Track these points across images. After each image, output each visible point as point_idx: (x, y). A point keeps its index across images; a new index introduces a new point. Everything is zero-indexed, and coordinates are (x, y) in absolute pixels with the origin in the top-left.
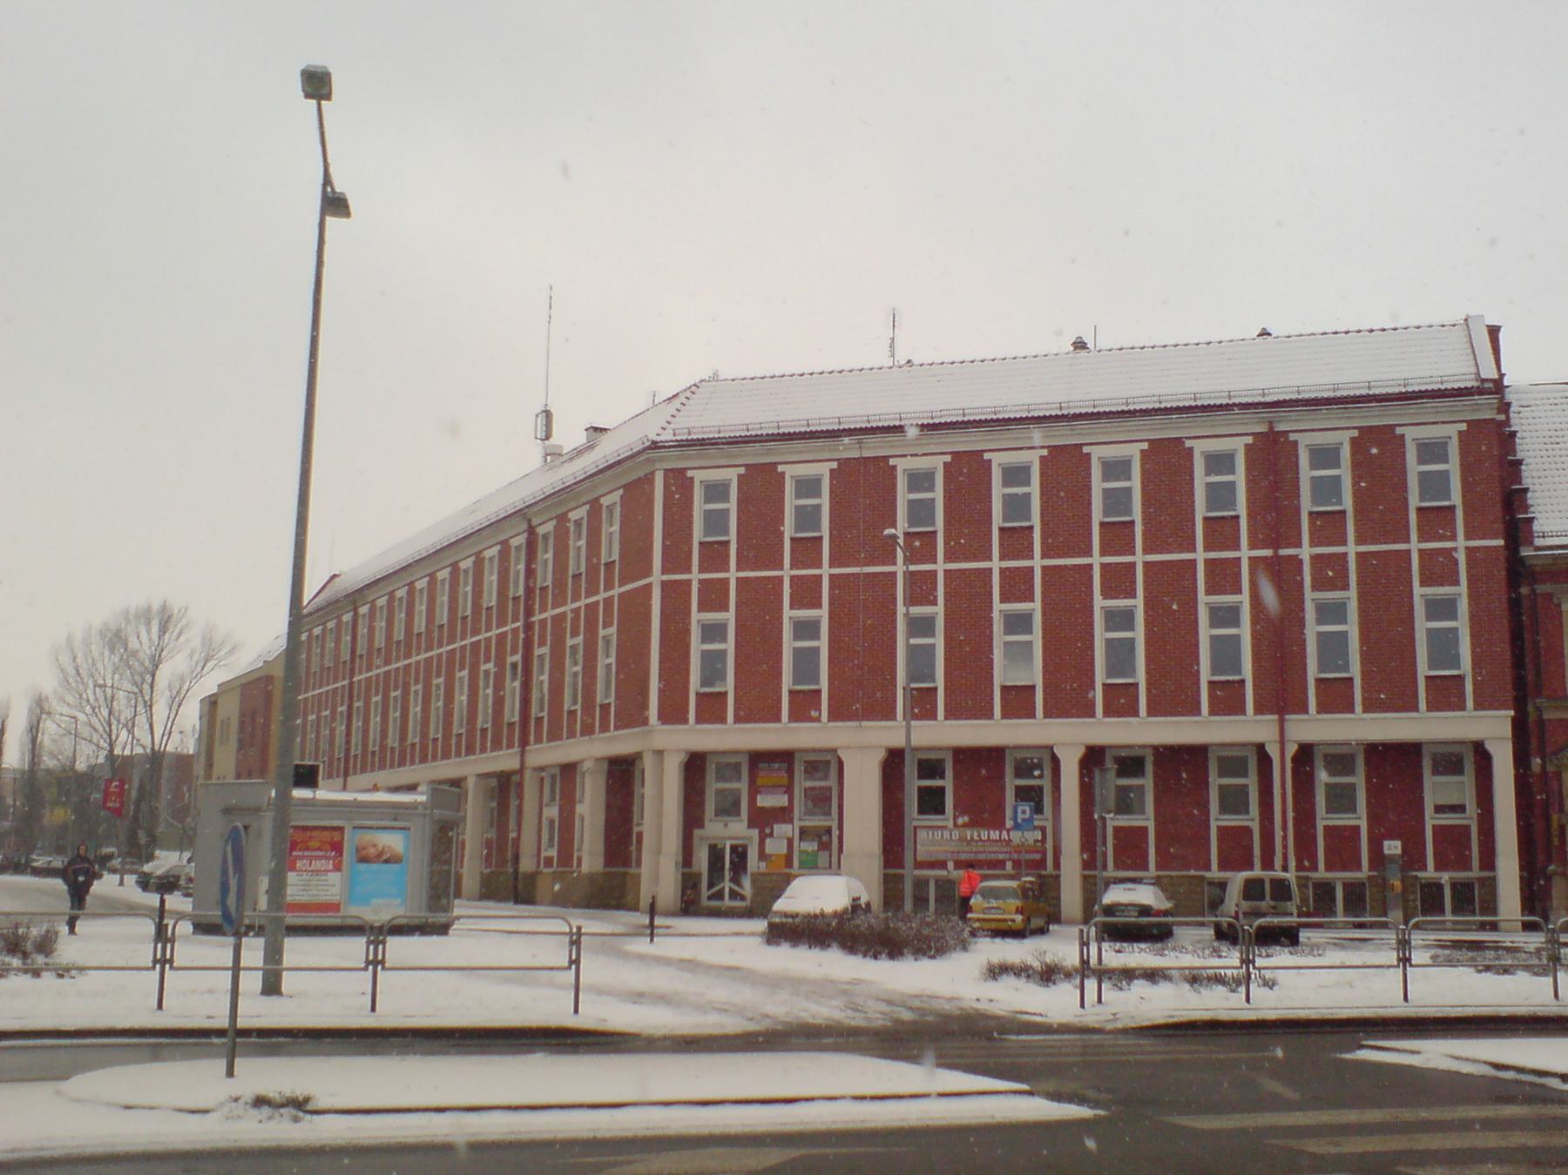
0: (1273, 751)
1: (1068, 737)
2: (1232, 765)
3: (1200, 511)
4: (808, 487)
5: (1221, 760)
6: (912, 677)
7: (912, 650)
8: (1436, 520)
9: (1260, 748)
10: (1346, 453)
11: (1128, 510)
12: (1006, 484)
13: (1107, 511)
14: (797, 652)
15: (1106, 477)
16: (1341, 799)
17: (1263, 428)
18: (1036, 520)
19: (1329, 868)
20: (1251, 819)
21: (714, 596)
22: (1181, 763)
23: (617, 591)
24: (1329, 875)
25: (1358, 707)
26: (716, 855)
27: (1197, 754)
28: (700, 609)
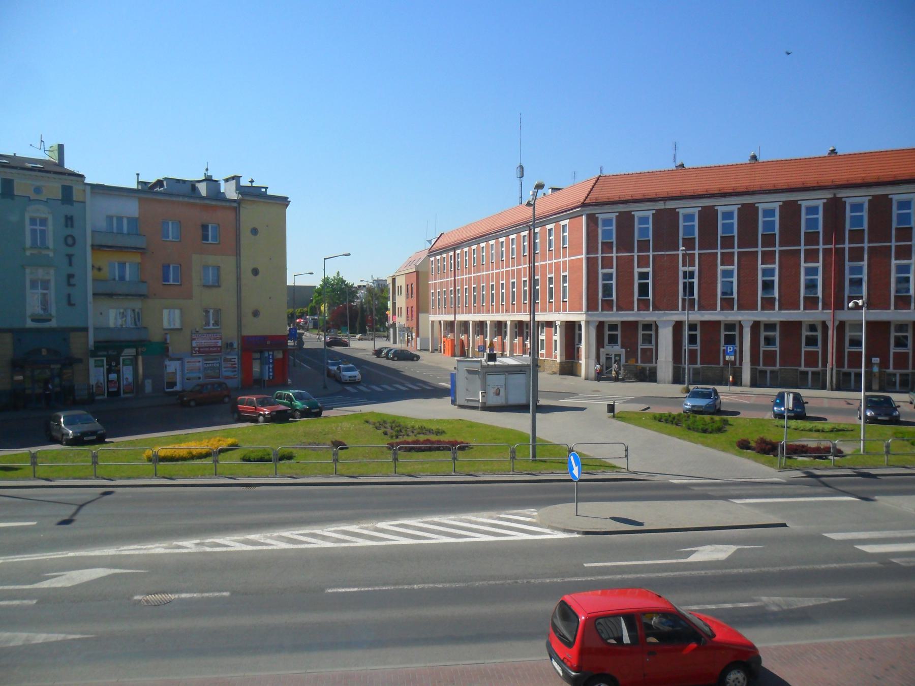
0: (830, 325)
1: (746, 318)
2: (812, 327)
3: (636, 237)
4: (644, 220)
5: (850, 325)
6: (723, 293)
7: (604, 286)
8: (857, 236)
9: (824, 324)
10: (866, 206)
11: (773, 229)
12: (764, 217)
13: (852, 225)
14: (640, 284)
15: (685, 221)
16: (769, 341)
17: (831, 196)
18: (735, 233)
19: (849, 367)
20: (819, 349)
21: (607, 263)
22: (791, 328)
23: (567, 259)
24: (895, 371)
25: (892, 307)
26: (608, 359)
27: (886, 325)
28: (602, 268)
